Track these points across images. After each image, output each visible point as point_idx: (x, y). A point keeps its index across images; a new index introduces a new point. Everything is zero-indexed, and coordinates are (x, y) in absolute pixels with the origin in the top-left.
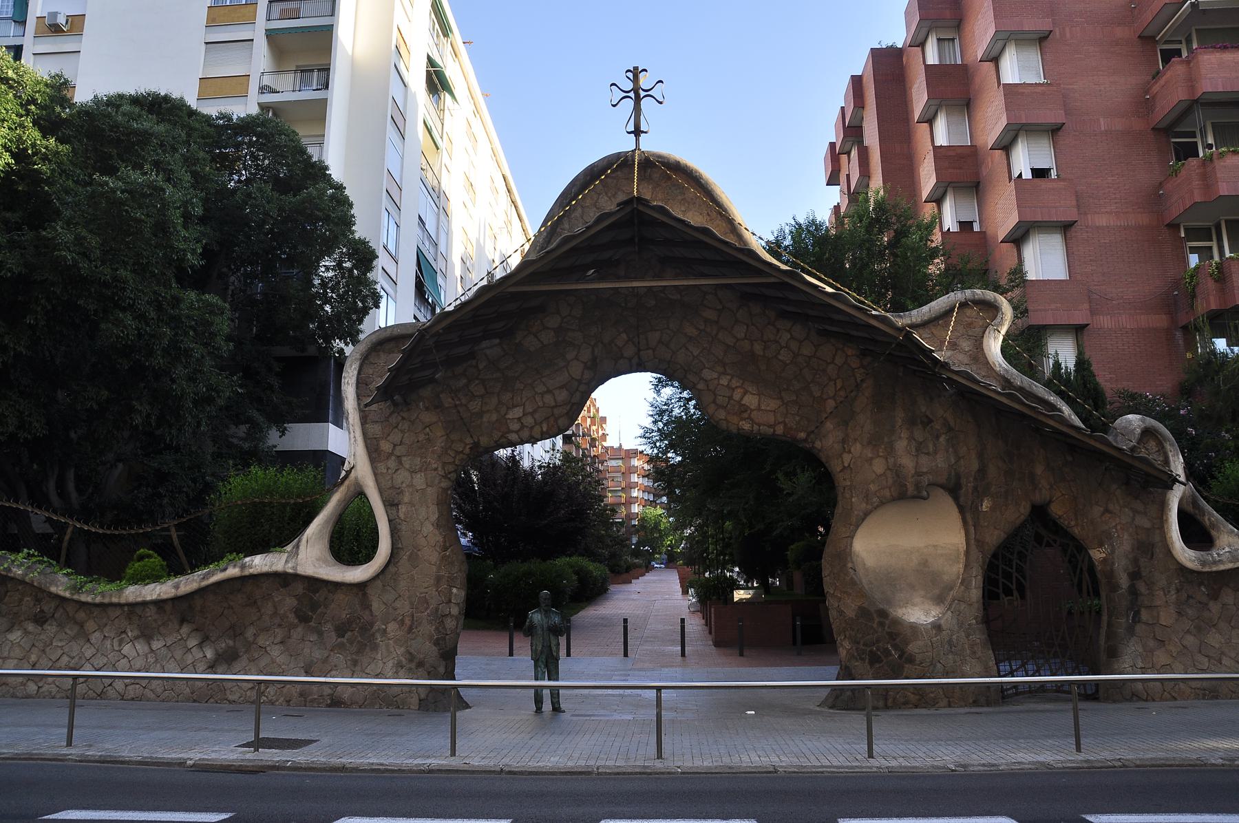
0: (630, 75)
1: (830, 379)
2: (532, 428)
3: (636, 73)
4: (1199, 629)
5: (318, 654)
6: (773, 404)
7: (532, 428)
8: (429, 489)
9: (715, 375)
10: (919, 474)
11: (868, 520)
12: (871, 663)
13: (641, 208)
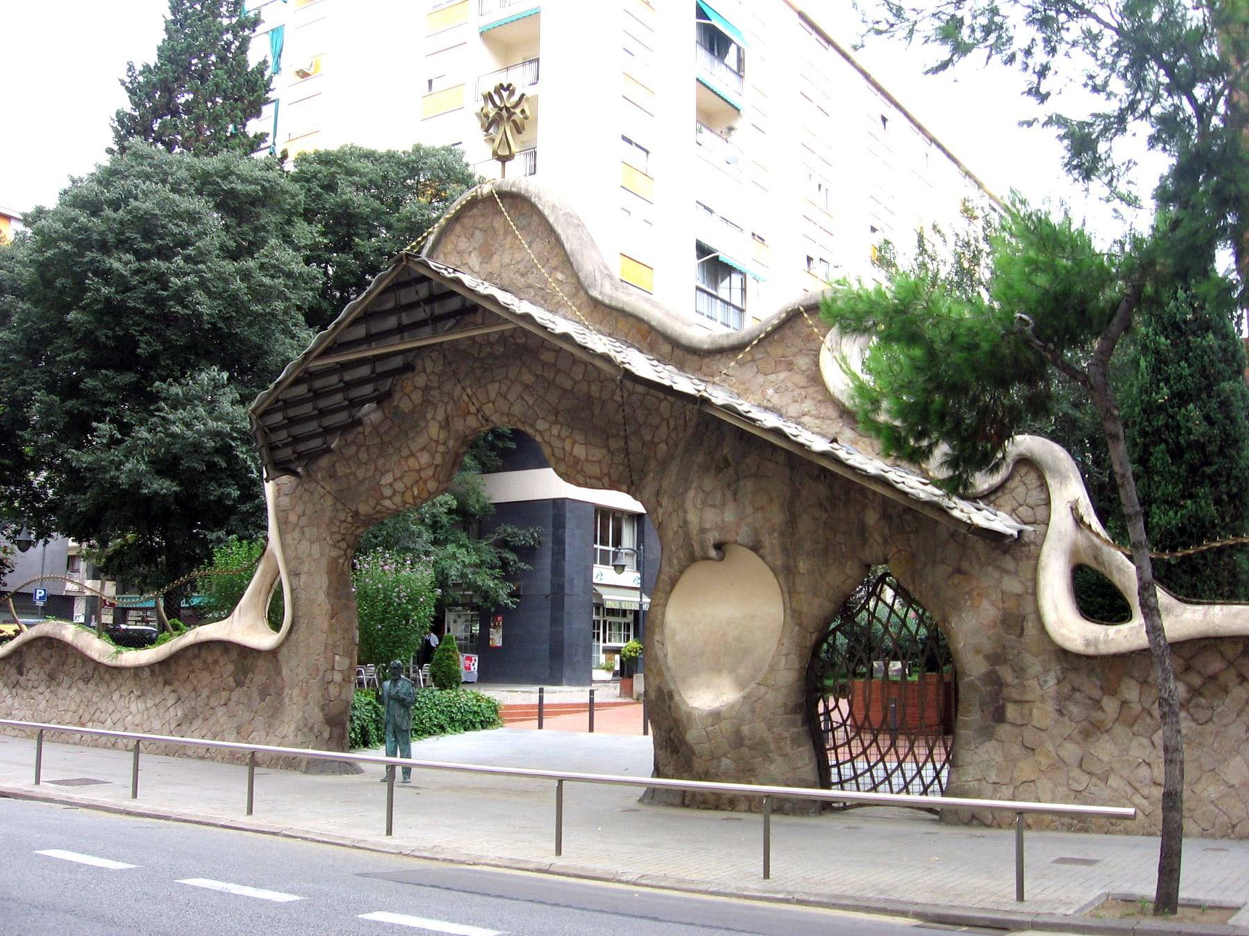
1: (663, 419)
6: (598, 453)
7: (403, 494)
10: (703, 531)
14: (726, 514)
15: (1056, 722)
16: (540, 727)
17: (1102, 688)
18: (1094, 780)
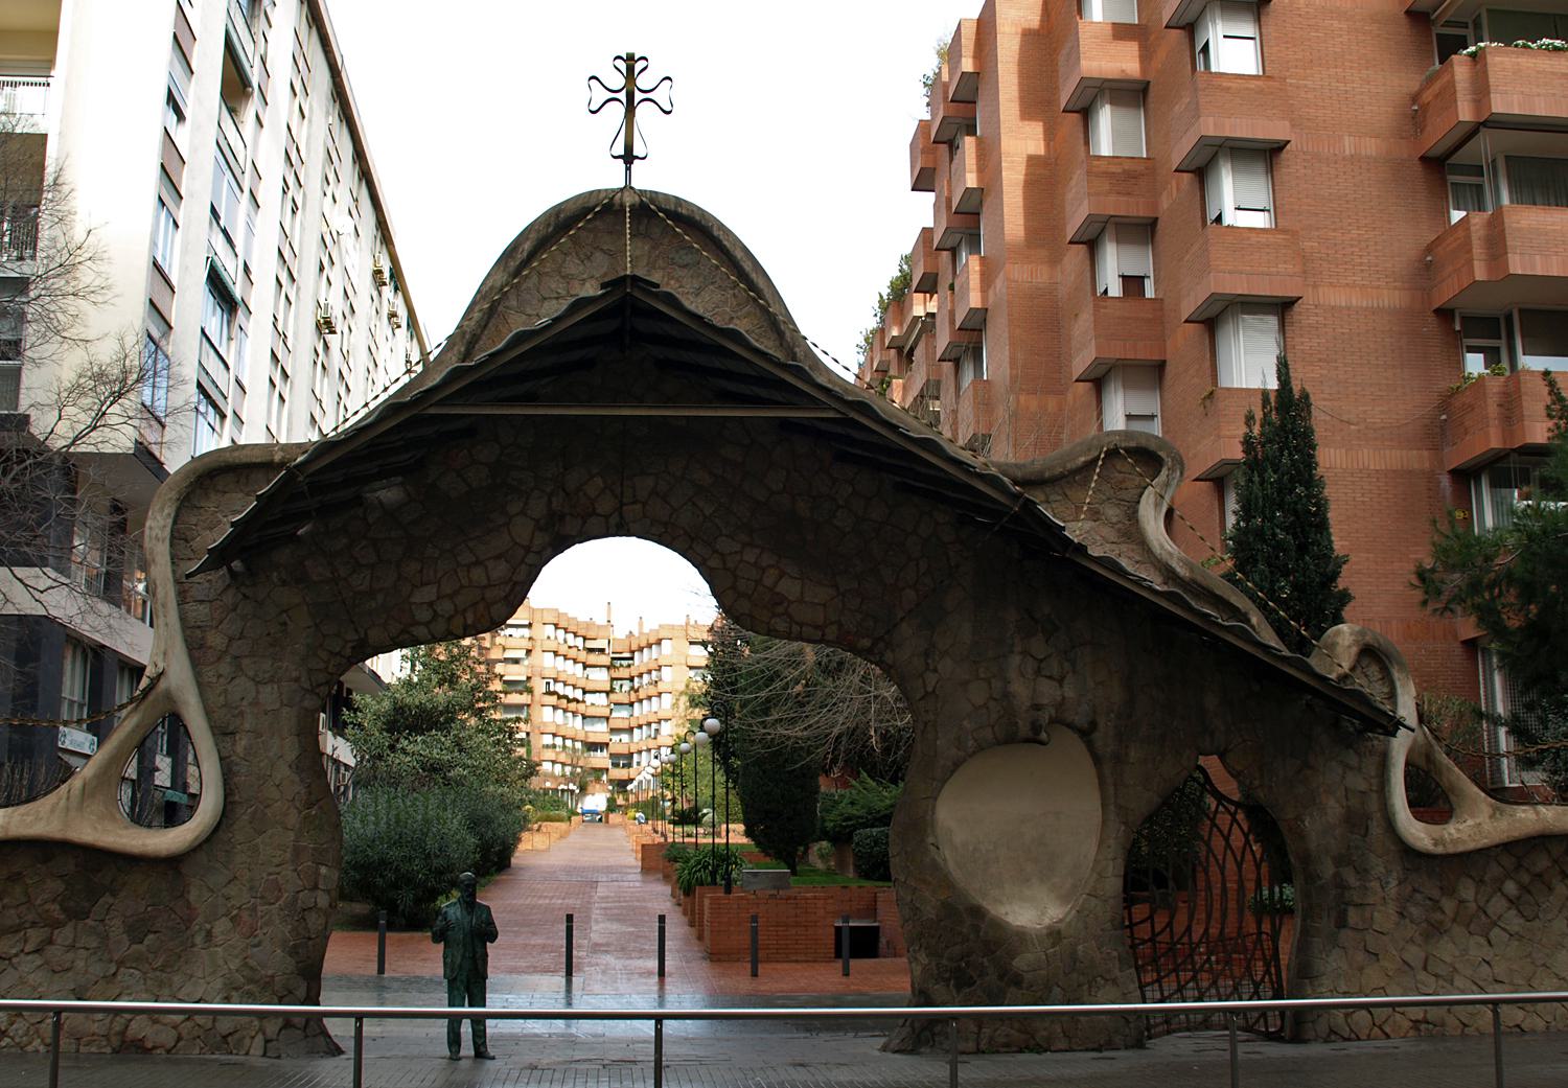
0: (622, 66)
2: (450, 618)
3: (630, 64)
4: (1427, 937)
5: (97, 969)
7: (450, 618)
8: (285, 710)
9: (737, 547)
11: (956, 774)
12: (959, 988)
13: (637, 294)
14: (1066, 689)
15: (1397, 924)
16: (755, 974)
17: (1441, 888)
18: (1441, 982)
